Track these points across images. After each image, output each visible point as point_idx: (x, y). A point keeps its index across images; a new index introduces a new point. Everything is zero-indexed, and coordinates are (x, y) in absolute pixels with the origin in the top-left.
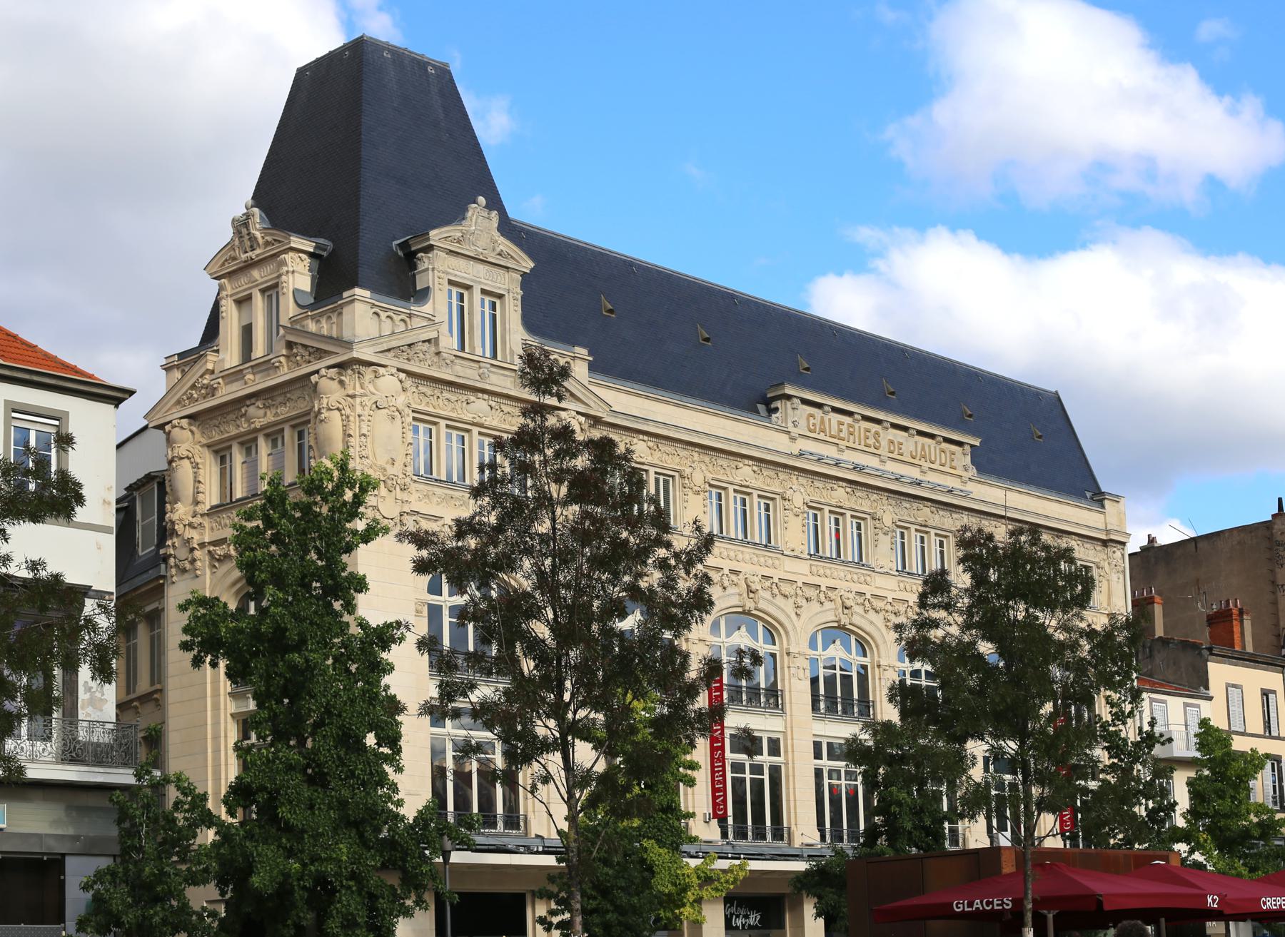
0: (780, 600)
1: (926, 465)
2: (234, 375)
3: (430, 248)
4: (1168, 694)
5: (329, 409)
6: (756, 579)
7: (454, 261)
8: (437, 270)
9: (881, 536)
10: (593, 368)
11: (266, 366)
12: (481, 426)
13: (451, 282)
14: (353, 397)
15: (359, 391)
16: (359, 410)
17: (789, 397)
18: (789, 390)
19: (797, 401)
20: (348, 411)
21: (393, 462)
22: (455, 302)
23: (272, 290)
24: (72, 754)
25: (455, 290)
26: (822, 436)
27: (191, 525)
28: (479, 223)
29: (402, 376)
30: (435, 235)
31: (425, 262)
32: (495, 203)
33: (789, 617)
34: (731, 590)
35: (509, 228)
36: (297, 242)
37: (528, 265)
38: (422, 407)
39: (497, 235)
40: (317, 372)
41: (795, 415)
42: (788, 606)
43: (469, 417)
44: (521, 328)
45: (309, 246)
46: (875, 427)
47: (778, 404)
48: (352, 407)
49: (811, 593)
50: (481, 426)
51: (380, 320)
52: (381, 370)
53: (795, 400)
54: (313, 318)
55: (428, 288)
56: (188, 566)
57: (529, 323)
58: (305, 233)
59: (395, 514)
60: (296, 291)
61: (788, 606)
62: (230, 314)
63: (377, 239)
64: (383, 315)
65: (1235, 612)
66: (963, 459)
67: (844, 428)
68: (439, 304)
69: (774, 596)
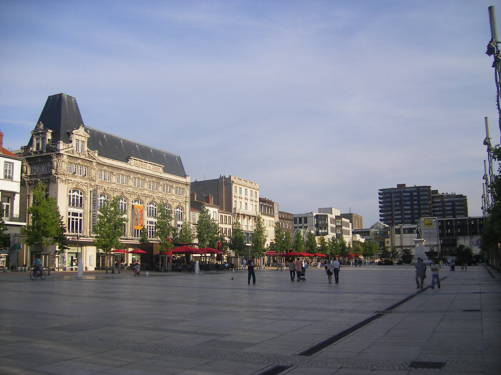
0: (127, 194)
1: (154, 170)
2: (35, 153)
3: (73, 134)
4: (196, 212)
5: (54, 161)
6: (124, 191)
7: (77, 136)
8: (74, 138)
9: (146, 183)
10: (98, 155)
11: (42, 152)
12: (79, 164)
13: (76, 139)
14: (59, 159)
15: (60, 158)
16: (60, 161)
17: (131, 159)
18: (131, 157)
19: (133, 159)
20: (58, 162)
21: (65, 171)
22: (76, 142)
23: (44, 139)
24: (12, 219)
25: (76, 140)
26: (137, 165)
27: (25, 177)
28: (81, 130)
29: (67, 156)
30: (74, 132)
31: (72, 136)
32: (83, 126)
33: (129, 197)
34: (119, 193)
35: (86, 130)
36: (49, 131)
37: (88, 136)
38: (70, 161)
39: (84, 131)
40: (52, 154)
41: (132, 161)
42: (129, 195)
43: (77, 163)
44: (87, 147)
45: (51, 131)
46: (146, 164)
47: (130, 160)
48: (59, 161)
49: (133, 193)
50: (79, 164)
51: (64, 146)
52: (64, 155)
53: (133, 159)
54: (51, 144)
55: (72, 140)
56: (24, 184)
57: (88, 146)
58: (51, 129)
59: (65, 179)
60: (49, 139)
61: (129, 195)
62: (35, 140)
63: (63, 132)
64: (64, 145)
65: (210, 196)
66: (161, 170)
67: (140, 164)
68: (74, 143)
69: (126, 194)
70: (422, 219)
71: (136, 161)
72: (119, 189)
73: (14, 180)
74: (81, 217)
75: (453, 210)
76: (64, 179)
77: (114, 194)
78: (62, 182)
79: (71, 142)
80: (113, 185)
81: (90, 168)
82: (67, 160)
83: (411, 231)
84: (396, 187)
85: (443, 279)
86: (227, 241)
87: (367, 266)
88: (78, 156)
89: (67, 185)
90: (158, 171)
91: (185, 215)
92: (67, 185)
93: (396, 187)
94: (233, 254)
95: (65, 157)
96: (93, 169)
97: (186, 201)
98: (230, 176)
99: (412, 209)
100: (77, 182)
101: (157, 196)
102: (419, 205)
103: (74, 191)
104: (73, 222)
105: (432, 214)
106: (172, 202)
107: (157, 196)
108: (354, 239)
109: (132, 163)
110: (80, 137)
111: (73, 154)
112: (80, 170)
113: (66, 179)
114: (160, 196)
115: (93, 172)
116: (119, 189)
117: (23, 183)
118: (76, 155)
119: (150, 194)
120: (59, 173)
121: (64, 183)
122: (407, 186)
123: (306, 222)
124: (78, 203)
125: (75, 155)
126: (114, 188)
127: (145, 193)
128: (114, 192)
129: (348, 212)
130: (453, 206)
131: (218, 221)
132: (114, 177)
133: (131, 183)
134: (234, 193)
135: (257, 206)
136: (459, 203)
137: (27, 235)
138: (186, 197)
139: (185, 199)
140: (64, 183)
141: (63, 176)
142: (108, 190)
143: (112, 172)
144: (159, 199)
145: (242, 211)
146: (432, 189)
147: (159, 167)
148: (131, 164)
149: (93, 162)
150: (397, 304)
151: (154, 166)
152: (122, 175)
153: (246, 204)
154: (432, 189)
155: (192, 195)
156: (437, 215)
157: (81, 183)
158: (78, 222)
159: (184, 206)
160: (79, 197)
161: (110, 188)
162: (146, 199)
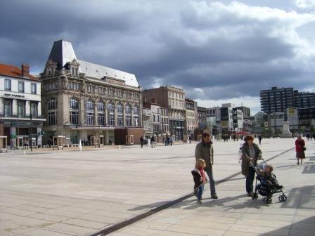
24: (38, 117)
68: (71, 70)
70: (288, 109)
75: (308, 103)
79: (69, 69)
83: (281, 116)
84: (152, 106)
85: (217, 164)
86: (246, 111)
87: (17, 98)
93: (152, 106)
94: (169, 134)
95: (67, 80)
99: (282, 103)
102: (286, 103)
105: (295, 105)
117: (42, 96)
118: (72, 77)
122: (126, 83)
123: (214, 113)
129: (240, 106)
130: (308, 100)
133: (106, 92)
134: (169, 96)
135: (34, 96)
136: (198, 147)
137: (37, 138)
146: (294, 90)
150: (159, 211)
154: (294, 90)
155: (143, 98)
156: (54, 106)
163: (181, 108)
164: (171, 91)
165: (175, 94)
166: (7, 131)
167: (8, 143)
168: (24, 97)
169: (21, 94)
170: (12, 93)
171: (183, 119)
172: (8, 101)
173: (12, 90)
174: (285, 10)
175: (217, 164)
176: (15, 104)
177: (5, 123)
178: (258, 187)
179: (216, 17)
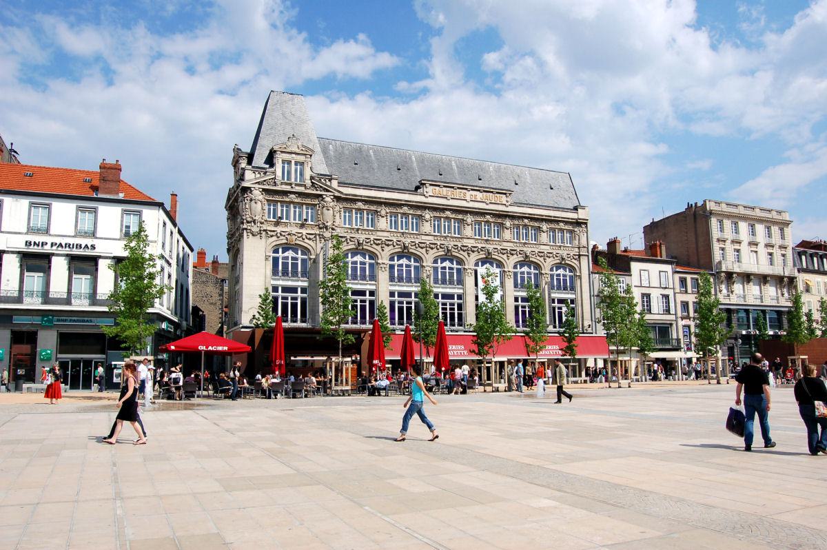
49: (433, 246)
71: (437, 188)
72: (395, 240)
73: (98, 236)
74: (682, 302)
76: (255, 229)
77: (383, 250)
78: (253, 235)
80: (542, 247)
81: (319, 207)
82: (261, 197)
85: (732, 400)
88: (288, 188)
89: (263, 239)
90: (498, 202)
91: (579, 281)
92: (263, 239)
95: (257, 194)
96: (324, 209)
97: (579, 256)
98: (705, 201)
100: (289, 234)
101: (499, 248)
103: (443, 260)
104: (401, 309)
106: (424, 249)
107: (499, 248)
108: (129, 531)
109: (427, 192)
110: (294, 155)
111: (275, 185)
112: (410, 223)
113: (260, 230)
114: (506, 248)
115: (328, 214)
116: (395, 240)
119: (480, 246)
120: (245, 221)
121: (259, 236)
124: (297, 269)
125: (280, 186)
126: (428, 243)
127: (464, 244)
128: (470, 252)
131: (674, 289)
132: (383, 221)
138: (579, 248)
139: (577, 250)
140: (259, 236)
141: (253, 224)
142: (534, 256)
143: (502, 223)
144: (503, 254)
145: (729, 265)
147: (498, 195)
148: (425, 194)
149: (324, 196)
151: (485, 194)
152: (562, 230)
153: (723, 249)
157: (300, 235)
158: (365, 305)
159: (575, 263)
160: (300, 260)
161: (536, 252)
162: (469, 256)
163: (777, 270)
164: (722, 216)
165: (760, 228)
166: (25, 338)
167: (22, 371)
168: (93, 247)
169: (89, 242)
170: (49, 240)
171: (785, 302)
172: (35, 261)
173: (52, 231)
174: (414, 99)
175: (732, 400)
176: (59, 266)
177: (17, 320)
178: (206, 380)
179: (361, 99)
